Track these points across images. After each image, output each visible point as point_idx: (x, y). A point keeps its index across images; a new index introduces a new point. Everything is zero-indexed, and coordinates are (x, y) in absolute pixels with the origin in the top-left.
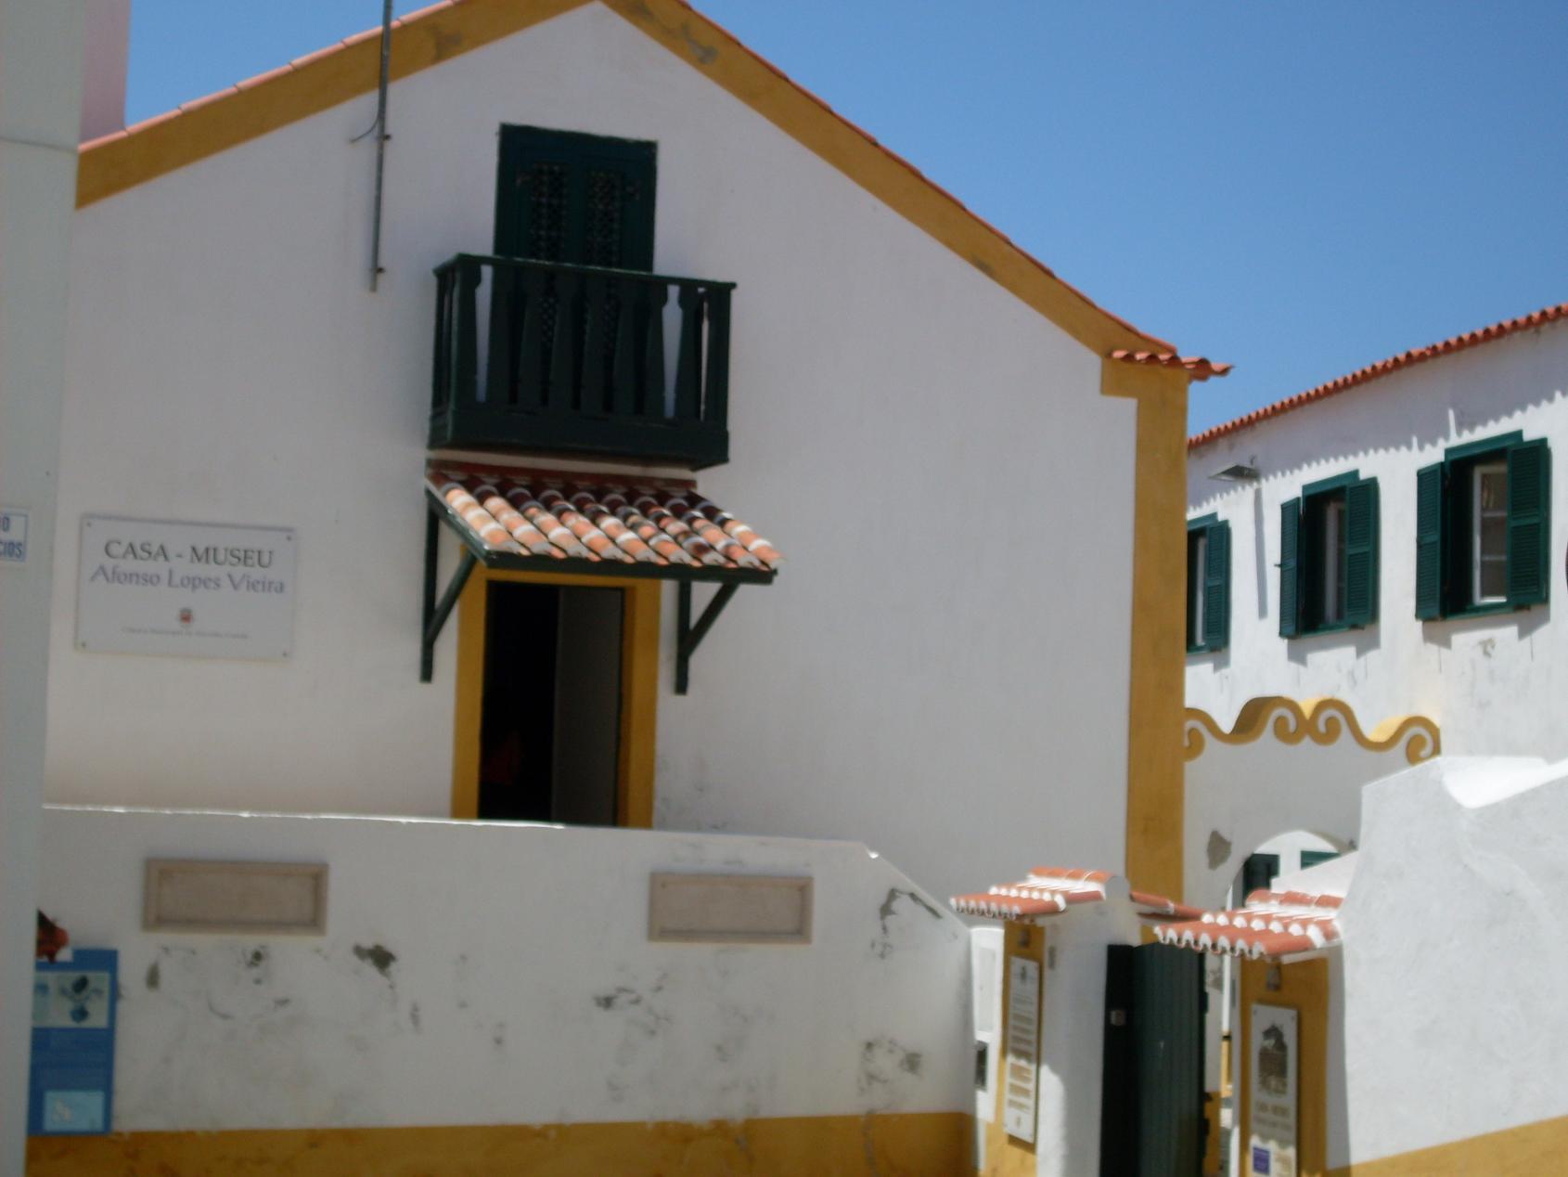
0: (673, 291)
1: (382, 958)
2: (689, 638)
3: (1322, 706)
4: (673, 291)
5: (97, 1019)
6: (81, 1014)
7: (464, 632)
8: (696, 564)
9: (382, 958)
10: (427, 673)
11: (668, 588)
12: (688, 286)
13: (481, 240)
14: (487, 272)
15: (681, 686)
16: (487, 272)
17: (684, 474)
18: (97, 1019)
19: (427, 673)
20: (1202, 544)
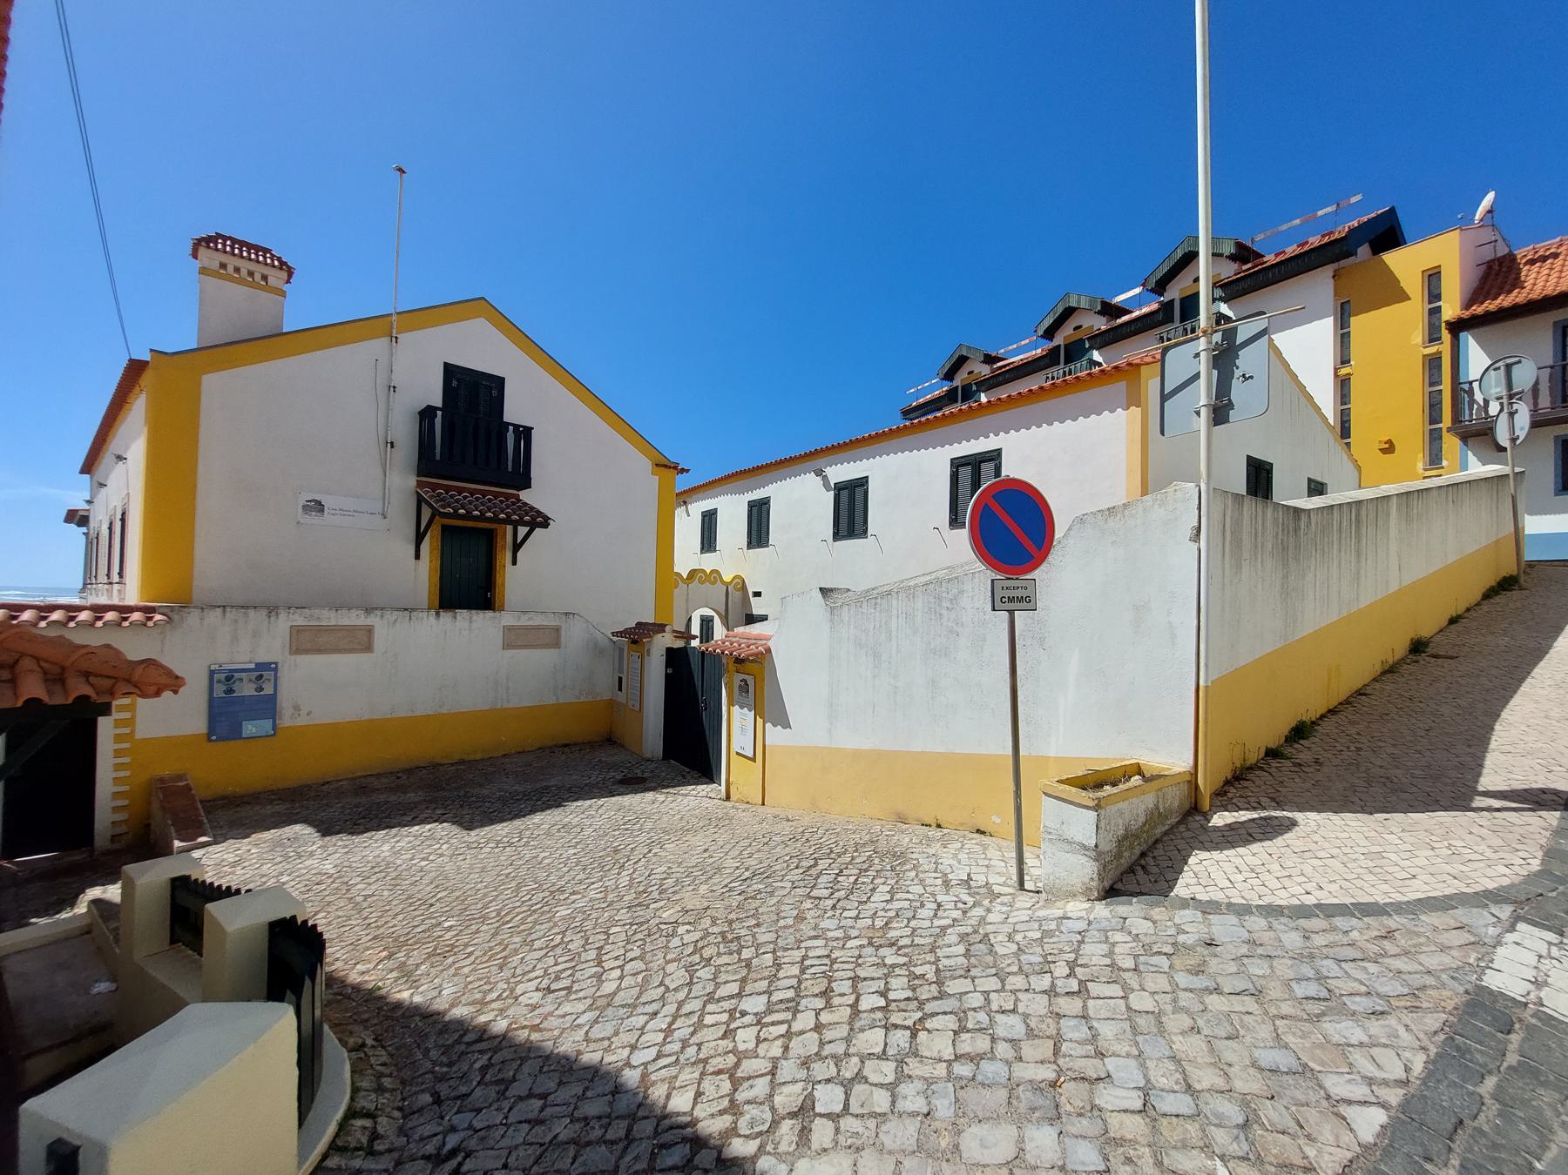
0: (511, 428)
1: (402, 171)
2: (517, 547)
3: (713, 571)
4: (511, 428)
5: (268, 690)
6: (261, 689)
7: (431, 538)
8: (58, 700)
9: (402, 171)
10: (417, 557)
11: (509, 528)
12: (516, 427)
13: (437, 401)
14: (439, 413)
15: (514, 563)
16: (439, 413)
17: (515, 492)
18: (268, 690)
19: (417, 557)
20: (755, 509)
